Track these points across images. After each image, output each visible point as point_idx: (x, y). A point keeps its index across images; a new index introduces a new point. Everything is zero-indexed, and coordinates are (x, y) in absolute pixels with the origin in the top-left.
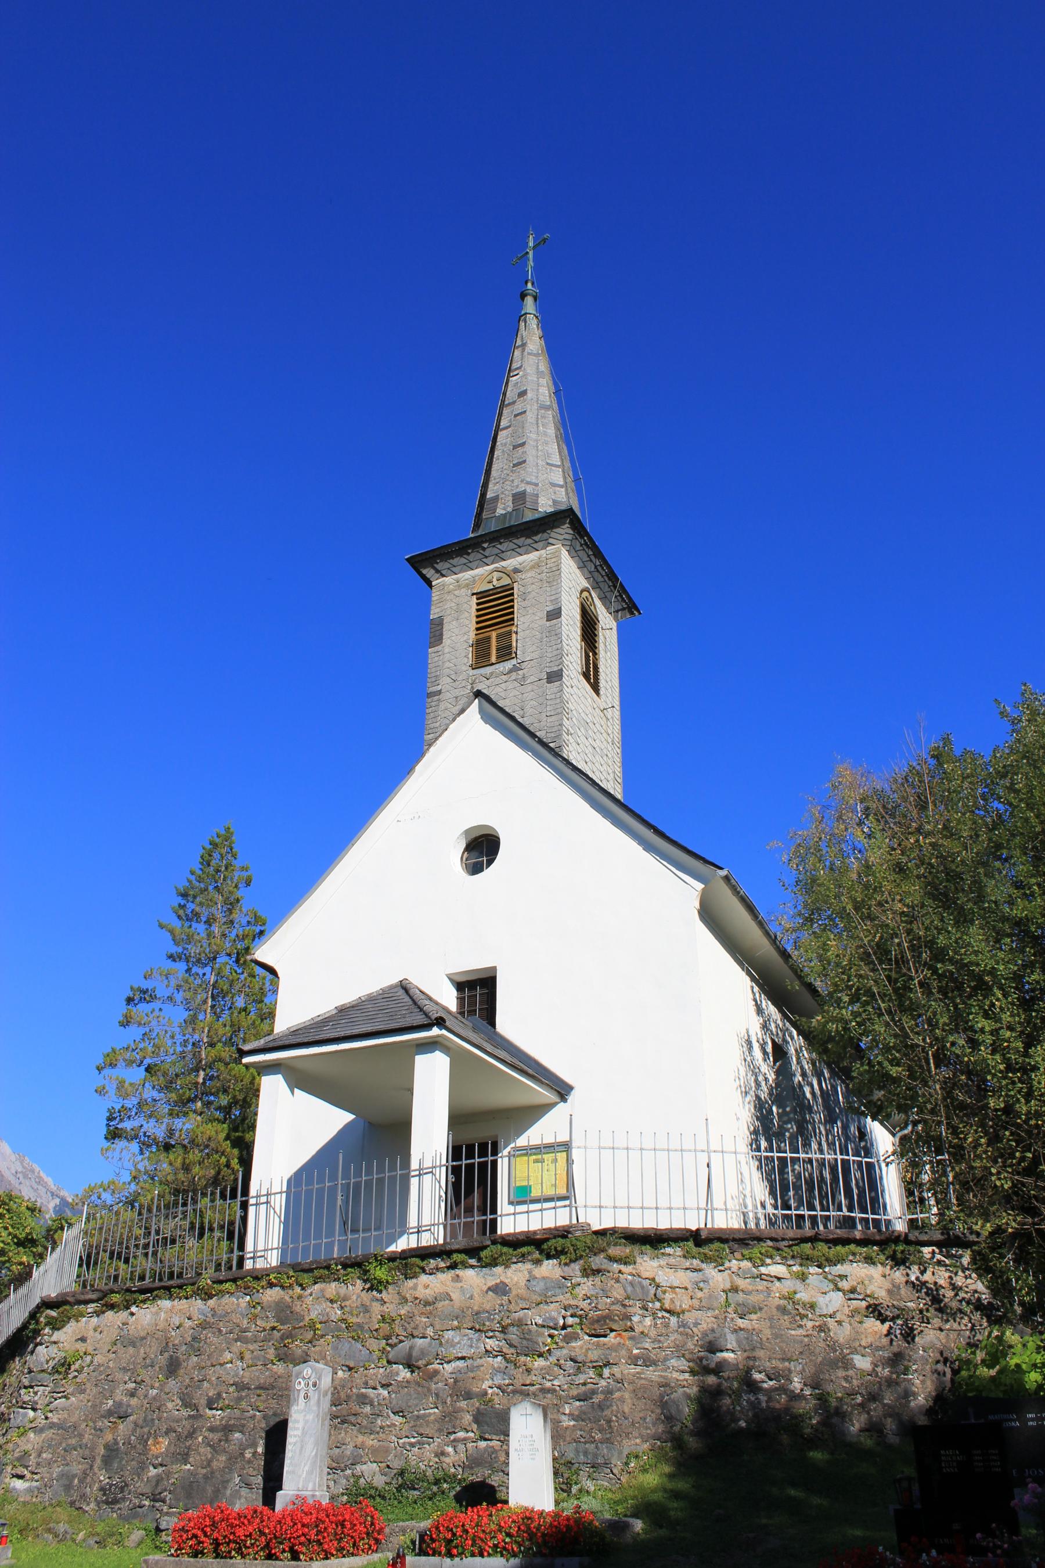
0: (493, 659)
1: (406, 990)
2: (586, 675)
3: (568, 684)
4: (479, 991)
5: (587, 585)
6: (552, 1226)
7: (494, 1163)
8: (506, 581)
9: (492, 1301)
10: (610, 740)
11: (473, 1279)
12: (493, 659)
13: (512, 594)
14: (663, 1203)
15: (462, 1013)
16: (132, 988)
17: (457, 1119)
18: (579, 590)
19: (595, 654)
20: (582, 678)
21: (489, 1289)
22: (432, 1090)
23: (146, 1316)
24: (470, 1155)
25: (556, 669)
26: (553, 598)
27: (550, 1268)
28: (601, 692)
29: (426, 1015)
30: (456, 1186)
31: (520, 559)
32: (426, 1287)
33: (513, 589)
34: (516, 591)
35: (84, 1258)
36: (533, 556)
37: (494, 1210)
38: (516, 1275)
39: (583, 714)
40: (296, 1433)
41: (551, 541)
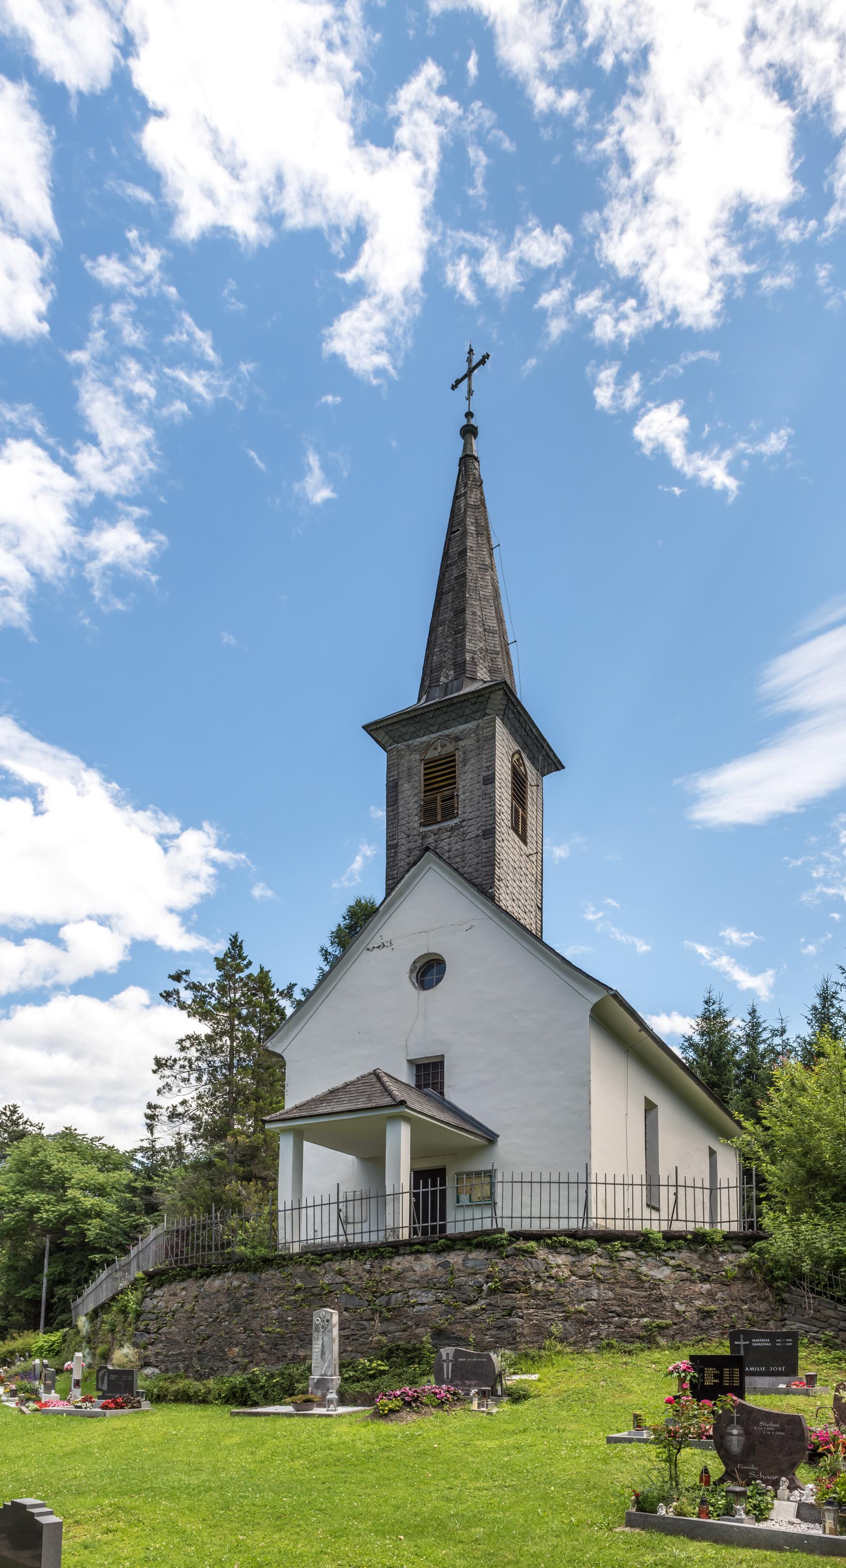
0: (439, 818)
1: (379, 1078)
2: (515, 829)
3: (500, 839)
4: (429, 1073)
5: (518, 748)
6: (480, 1229)
7: (443, 1193)
8: (450, 748)
9: (441, 1271)
10: (534, 880)
11: (429, 1261)
12: (439, 818)
13: (454, 761)
14: (554, 1213)
15: (418, 1086)
16: (155, 1072)
17: (419, 1176)
18: (511, 753)
19: (524, 809)
20: (511, 831)
21: (439, 1265)
22: (400, 1143)
23: (216, 1283)
24: (434, 1228)
25: (489, 827)
26: (488, 764)
27: (478, 1255)
28: (529, 839)
29: (394, 1099)
30: (416, 1204)
31: (461, 728)
32: (398, 1264)
33: (454, 755)
34: (457, 757)
35: (169, 1248)
36: (472, 725)
37: (443, 1217)
38: (455, 1258)
39: (512, 862)
40: (316, 1350)
41: (487, 711)
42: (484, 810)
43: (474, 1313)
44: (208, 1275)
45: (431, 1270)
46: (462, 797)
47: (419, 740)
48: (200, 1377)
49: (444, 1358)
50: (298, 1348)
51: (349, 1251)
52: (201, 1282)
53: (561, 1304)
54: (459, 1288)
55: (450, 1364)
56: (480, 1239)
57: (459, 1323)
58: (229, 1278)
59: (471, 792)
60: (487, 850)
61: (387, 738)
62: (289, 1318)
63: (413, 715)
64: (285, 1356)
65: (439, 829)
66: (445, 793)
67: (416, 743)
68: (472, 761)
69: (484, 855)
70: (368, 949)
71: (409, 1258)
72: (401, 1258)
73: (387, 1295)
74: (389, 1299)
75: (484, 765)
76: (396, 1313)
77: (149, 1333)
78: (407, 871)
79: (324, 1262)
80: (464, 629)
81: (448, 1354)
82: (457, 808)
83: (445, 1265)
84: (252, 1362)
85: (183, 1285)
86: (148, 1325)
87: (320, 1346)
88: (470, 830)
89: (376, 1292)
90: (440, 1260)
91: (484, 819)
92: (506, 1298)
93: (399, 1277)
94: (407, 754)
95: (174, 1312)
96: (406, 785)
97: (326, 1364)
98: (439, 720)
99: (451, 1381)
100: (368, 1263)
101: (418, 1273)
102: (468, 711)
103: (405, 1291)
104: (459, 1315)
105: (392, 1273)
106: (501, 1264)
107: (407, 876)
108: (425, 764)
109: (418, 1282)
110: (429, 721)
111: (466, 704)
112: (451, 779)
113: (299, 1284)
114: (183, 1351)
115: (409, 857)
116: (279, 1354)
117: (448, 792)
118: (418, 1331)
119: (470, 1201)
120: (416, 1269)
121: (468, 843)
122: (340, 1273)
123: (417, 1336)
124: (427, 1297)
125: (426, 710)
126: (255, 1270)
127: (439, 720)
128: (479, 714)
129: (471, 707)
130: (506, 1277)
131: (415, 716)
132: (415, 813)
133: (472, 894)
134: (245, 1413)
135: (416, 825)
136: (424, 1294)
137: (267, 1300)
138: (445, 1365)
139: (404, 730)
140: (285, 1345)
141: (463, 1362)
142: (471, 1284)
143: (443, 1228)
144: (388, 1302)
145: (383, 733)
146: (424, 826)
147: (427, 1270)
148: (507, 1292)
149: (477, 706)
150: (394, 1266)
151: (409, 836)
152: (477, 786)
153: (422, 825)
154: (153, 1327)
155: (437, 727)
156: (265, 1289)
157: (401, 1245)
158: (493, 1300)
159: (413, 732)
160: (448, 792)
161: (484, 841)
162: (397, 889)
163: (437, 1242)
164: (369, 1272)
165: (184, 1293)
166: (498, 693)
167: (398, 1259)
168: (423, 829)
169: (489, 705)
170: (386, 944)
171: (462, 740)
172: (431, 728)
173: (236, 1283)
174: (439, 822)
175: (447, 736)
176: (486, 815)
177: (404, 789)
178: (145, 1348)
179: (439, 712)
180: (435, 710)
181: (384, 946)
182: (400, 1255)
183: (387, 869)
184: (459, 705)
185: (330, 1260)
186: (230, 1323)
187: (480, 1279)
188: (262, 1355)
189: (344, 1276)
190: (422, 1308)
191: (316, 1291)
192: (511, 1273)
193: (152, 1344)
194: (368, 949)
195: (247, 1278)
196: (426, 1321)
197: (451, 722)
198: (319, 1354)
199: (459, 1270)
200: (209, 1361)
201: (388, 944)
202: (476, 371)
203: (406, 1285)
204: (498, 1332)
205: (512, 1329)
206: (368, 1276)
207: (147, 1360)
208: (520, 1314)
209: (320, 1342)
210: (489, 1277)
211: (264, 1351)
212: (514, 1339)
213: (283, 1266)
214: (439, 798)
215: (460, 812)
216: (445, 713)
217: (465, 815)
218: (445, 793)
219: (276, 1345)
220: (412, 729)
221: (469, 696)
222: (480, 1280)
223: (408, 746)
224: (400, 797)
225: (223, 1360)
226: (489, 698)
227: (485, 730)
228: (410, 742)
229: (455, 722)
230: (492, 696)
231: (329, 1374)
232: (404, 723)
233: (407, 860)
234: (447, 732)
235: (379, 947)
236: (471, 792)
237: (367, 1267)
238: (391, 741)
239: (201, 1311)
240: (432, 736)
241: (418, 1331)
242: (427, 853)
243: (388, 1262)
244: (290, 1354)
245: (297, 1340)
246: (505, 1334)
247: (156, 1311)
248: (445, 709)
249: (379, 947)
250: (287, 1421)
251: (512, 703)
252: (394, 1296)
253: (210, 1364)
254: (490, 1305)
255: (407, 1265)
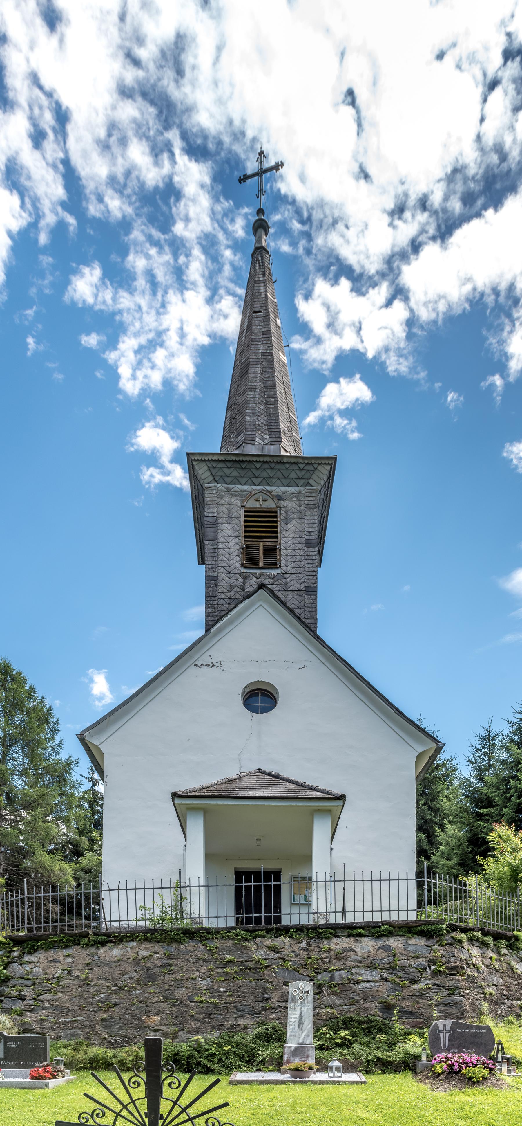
9: (382, 954)
21: (379, 948)
25: (312, 585)
31: (283, 489)
32: (337, 944)
41: (311, 481)
42: (306, 569)
43: (421, 992)
44: (103, 944)
45: (373, 952)
46: (284, 552)
47: (240, 487)
48: (112, 1045)
49: (441, 1029)
50: (236, 1018)
51: (284, 929)
52: (93, 950)
53: (481, 987)
54: (403, 969)
55: (447, 1035)
56: (423, 927)
57: (408, 999)
58: (133, 948)
59: (294, 550)
60: (310, 605)
61: (208, 474)
62: (222, 989)
63: (241, 459)
64: (223, 1025)
65: (261, 575)
66: (267, 543)
67: (236, 489)
68: (294, 522)
69: (306, 609)
70: (196, 665)
71: (348, 940)
72: (339, 939)
73: (330, 972)
74: (333, 975)
75: (306, 529)
76: (343, 989)
77: (23, 1000)
78: (241, 602)
79: (255, 938)
80: (276, 401)
81: (445, 1026)
82: (280, 560)
83: (387, 948)
84: (182, 1030)
85: (69, 951)
86: (23, 991)
87: (298, 1016)
88: (292, 583)
89: (317, 969)
90: (381, 943)
91: (307, 577)
92: (451, 980)
93: (338, 956)
94: (228, 496)
95: (58, 978)
96: (226, 525)
97: (304, 1033)
98: (264, 474)
99: (448, 1050)
100: (304, 942)
101: (359, 953)
102: (293, 475)
103: (349, 969)
104: (406, 992)
105: (332, 952)
106: (440, 952)
107: (240, 606)
108: (245, 511)
109: (361, 961)
110: (254, 471)
111: (294, 467)
112: (273, 534)
113: (229, 957)
114: (81, 1018)
115: (230, 592)
116: (214, 1023)
117: (270, 543)
118: (366, 1005)
119: (305, 900)
120: (356, 950)
121: (291, 594)
122: (275, 949)
123: (366, 1009)
124: (367, 975)
125: (255, 459)
126: (174, 940)
127: (264, 474)
128: (302, 482)
129: (298, 472)
130: (448, 962)
131: (243, 461)
132: (236, 553)
133: (305, 638)
134: (300, 1082)
135: (237, 564)
136: (368, 972)
137: (192, 971)
138: (442, 1035)
139: (227, 471)
140: (220, 1014)
141: (460, 1033)
142: (415, 966)
143: (278, 920)
144: (332, 978)
145: (206, 468)
146: (245, 568)
147: (369, 951)
148: (451, 975)
149: (304, 472)
150: (333, 946)
151: (229, 573)
152: (299, 546)
153: (244, 566)
154: (28, 993)
155: (260, 480)
156: (188, 960)
157: (339, 928)
158: (439, 980)
159: (236, 477)
160: (270, 543)
161: (306, 597)
162: (229, 616)
163: (380, 927)
164: (306, 950)
165: (69, 960)
166: (325, 466)
167: (335, 940)
168: (243, 570)
169: (314, 477)
170: (217, 665)
171: (284, 500)
172: (254, 480)
173: (143, 953)
174: (260, 568)
175: (270, 492)
176: (308, 574)
177: (224, 528)
178: (21, 1015)
179: (266, 466)
180: (264, 462)
181: (213, 665)
182: (338, 937)
183: (207, 597)
184: (287, 466)
185: (263, 937)
186: (143, 992)
187: (424, 962)
188: (194, 1024)
189: (278, 952)
190: (368, 985)
191: (250, 965)
192: (452, 959)
193: (31, 1011)
194: (196, 665)
195: (160, 949)
196: (373, 997)
197: (274, 480)
198: (297, 1023)
199: (401, 953)
200: (120, 1029)
201: (218, 664)
202: (250, 180)
203: (348, 964)
204: (446, 1008)
205: (460, 1006)
206: (305, 953)
207: (27, 1027)
208: (462, 994)
209: (298, 1012)
210: (432, 961)
211: (196, 1020)
212: (462, 1014)
213: (207, 939)
214: (261, 548)
215: (282, 565)
216: (272, 469)
217: (288, 569)
218: (267, 543)
219: (210, 1014)
220: (235, 473)
221: (300, 461)
222: (423, 963)
223: (229, 490)
224: (220, 534)
225: (140, 1028)
226: (316, 469)
227: (307, 499)
228: (231, 486)
229: (278, 481)
230: (320, 468)
231: (308, 1042)
232: (229, 465)
233: (228, 594)
234: (269, 488)
235: (208, 665)
236: (294, 550)
237: (304, 945)
238: (211, 478)
239: (99, 979)
240: (254, 487)
241: (366, 1005)
242: (261, 591)
243: (326, 942)
244: (227, 1024)
245: (234, 1010)
246: (453, 1010)
247: (30, 977)
248: (273, 465)
249: (208, 665)
250: (352, 1090)
251: (329, 483)
252: (337, 974)
253: (123, 1032)
254: (434, 984)
255: (347, 946)
